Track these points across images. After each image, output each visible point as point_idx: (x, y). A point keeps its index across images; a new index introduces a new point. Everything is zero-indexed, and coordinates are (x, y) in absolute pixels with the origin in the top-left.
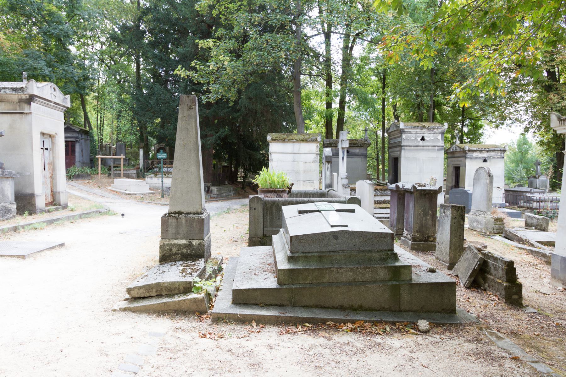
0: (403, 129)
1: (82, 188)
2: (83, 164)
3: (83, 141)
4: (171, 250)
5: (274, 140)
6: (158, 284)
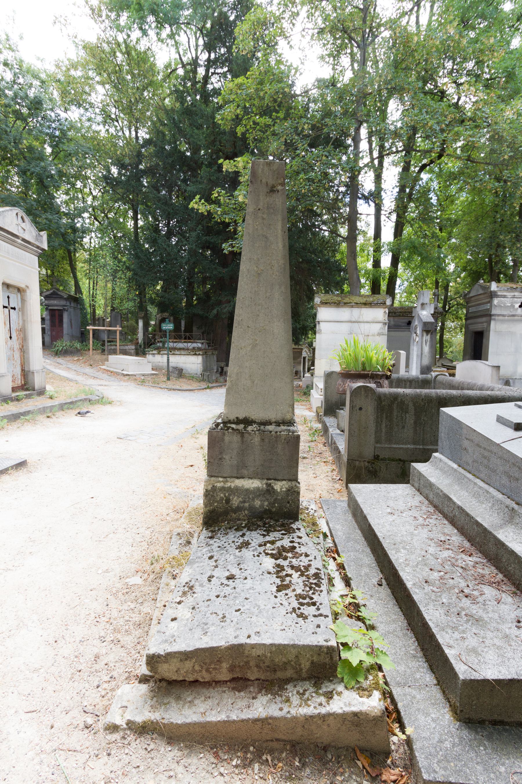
0: (495, 292)
1: (70, 366)
2: (72, 338)
3: (71, 310)
4: (228, 501)
5: (324, 303)
6: (236, 650)
